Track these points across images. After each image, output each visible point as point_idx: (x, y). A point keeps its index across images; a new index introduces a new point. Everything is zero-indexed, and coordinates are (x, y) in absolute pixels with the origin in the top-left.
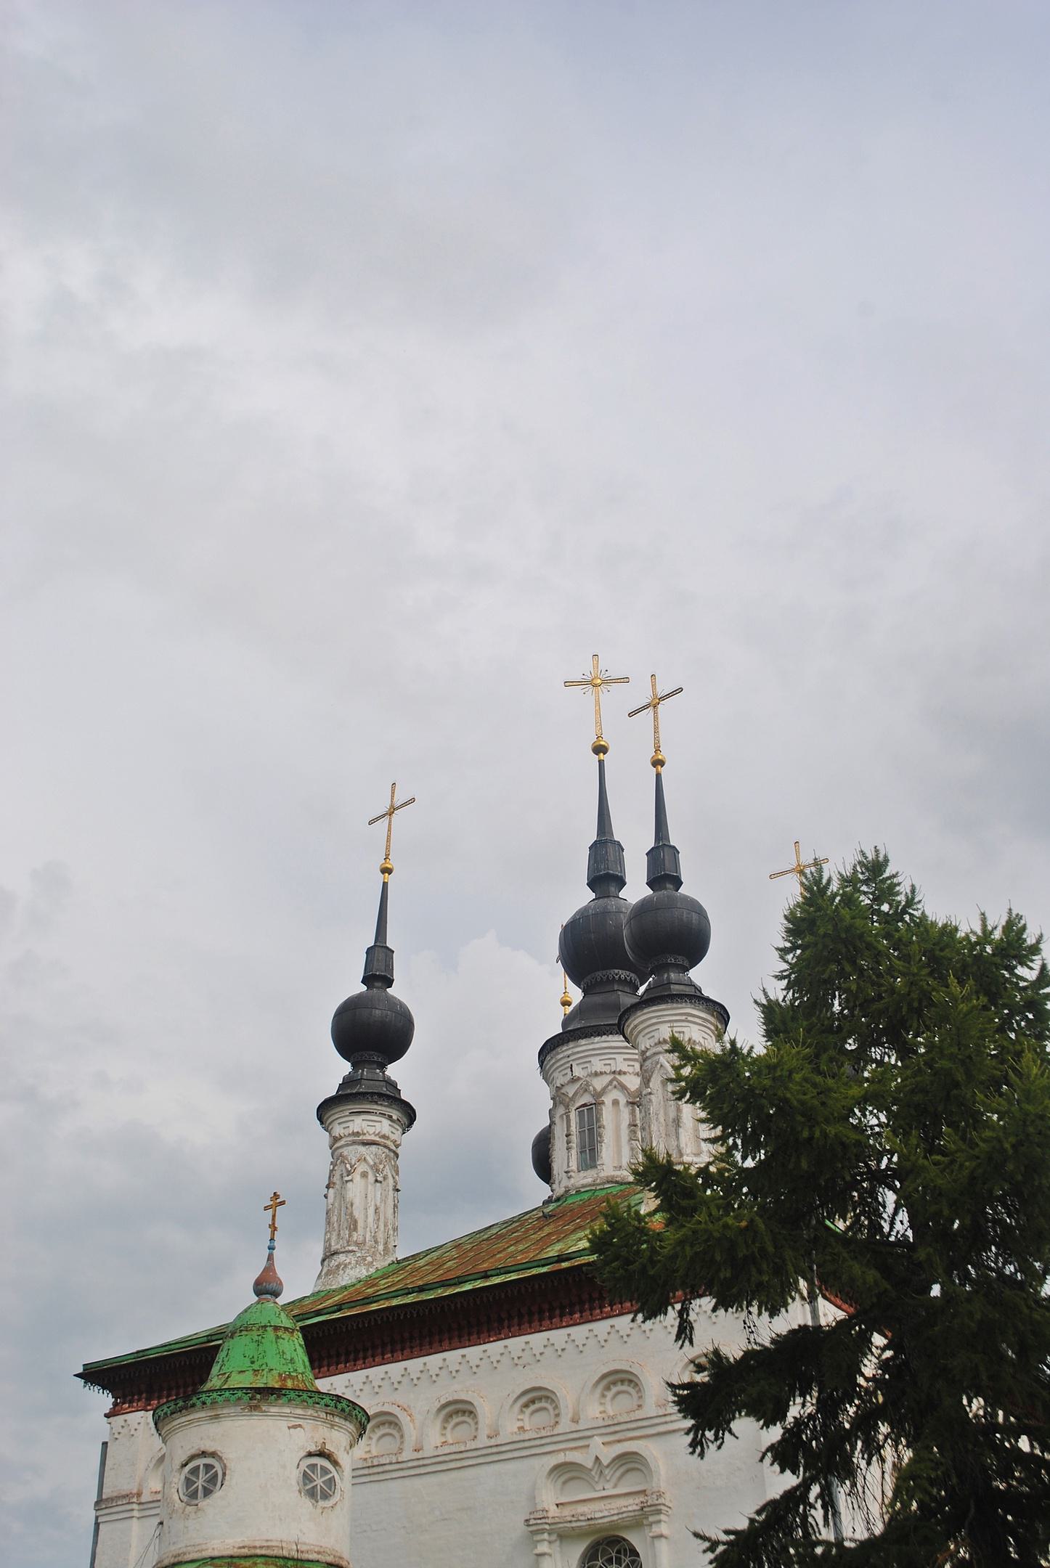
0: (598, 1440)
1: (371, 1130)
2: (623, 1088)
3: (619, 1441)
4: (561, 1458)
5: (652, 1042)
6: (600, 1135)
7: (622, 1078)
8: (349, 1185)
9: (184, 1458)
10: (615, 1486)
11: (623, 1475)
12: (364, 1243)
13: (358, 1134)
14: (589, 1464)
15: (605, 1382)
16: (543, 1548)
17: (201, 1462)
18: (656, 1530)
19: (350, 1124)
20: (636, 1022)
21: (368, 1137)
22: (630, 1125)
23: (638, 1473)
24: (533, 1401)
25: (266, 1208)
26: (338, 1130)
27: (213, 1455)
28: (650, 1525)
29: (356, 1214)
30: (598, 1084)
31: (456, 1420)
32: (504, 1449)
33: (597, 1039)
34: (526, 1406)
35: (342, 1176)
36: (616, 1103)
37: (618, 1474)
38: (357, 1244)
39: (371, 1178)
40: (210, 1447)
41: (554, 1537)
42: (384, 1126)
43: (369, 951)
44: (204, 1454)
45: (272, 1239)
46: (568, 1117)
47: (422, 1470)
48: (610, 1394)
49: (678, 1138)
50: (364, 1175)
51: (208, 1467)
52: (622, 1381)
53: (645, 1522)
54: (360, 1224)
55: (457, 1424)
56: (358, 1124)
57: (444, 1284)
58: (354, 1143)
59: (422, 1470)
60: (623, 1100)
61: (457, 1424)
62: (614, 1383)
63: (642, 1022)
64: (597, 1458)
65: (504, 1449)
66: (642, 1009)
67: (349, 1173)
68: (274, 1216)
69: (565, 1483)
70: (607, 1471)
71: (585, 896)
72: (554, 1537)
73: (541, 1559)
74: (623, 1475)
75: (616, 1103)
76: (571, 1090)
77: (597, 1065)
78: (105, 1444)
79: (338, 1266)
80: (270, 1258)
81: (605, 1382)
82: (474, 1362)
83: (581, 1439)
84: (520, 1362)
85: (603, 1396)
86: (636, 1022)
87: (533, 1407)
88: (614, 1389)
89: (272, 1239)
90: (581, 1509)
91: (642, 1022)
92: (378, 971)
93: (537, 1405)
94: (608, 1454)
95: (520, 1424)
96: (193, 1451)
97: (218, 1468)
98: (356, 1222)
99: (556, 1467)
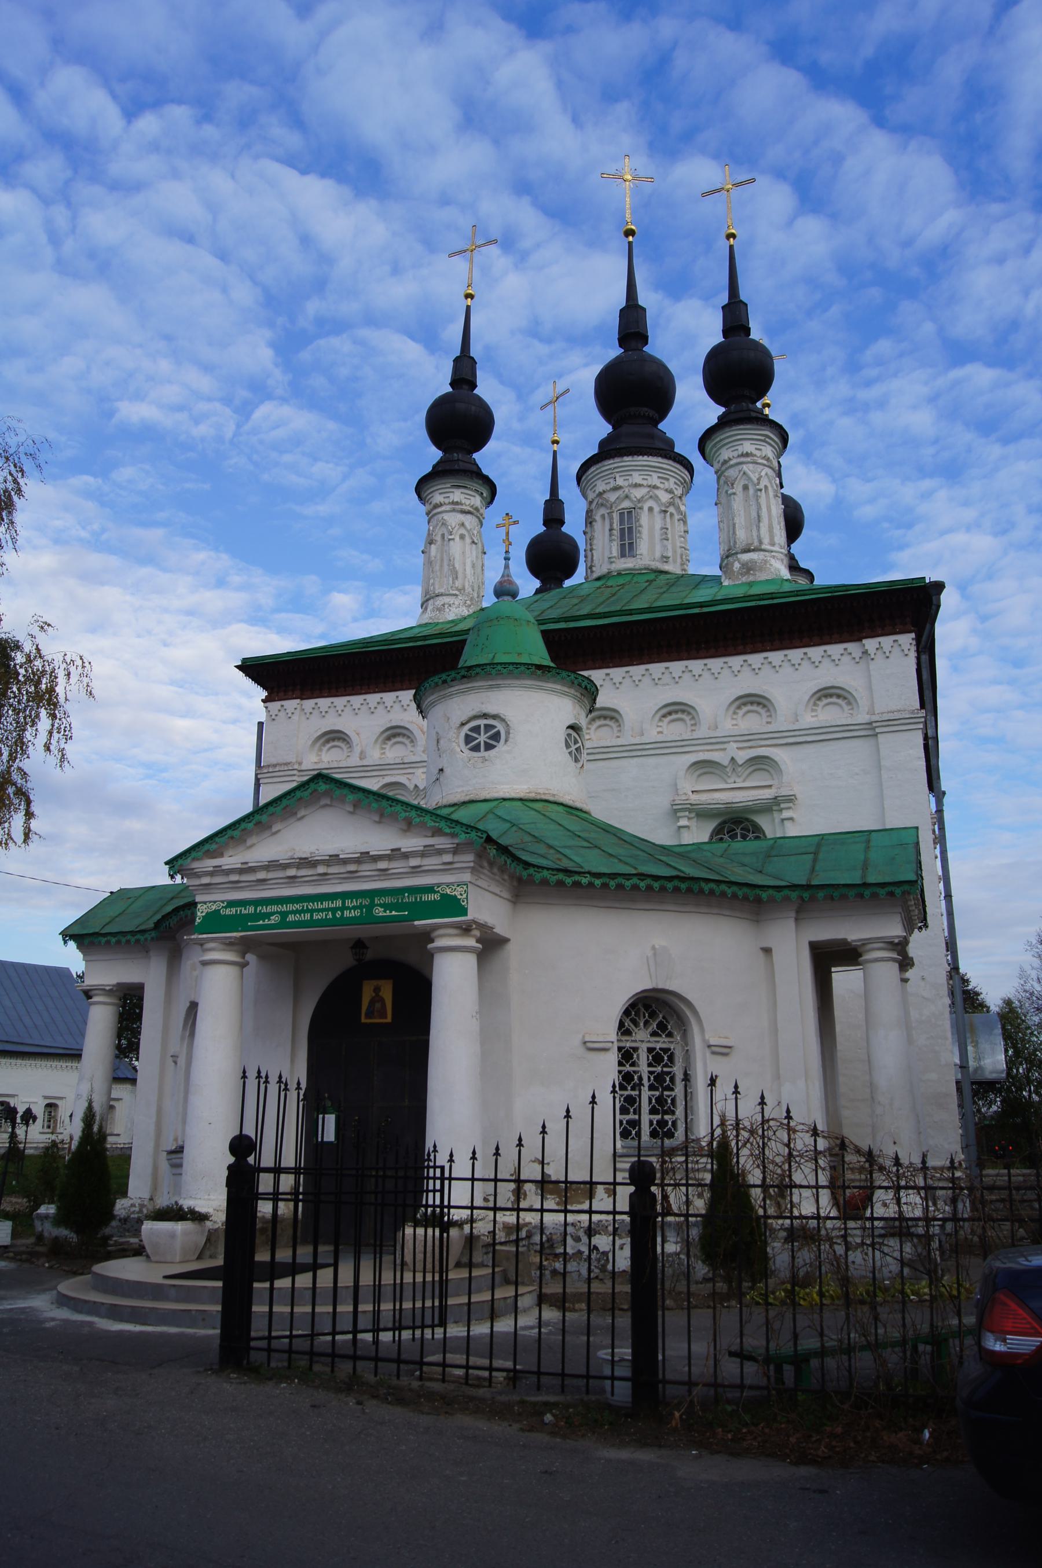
0: (735, 745)
1: (468, 502)
2: (656, 498)
3: (750, 747)
4: (702, 756)
5: (735, 454)
6: (640, 532)
7: (657, 492)
8: (451, 542)
9: (464, 718)
10: (744, 781)
11: (750, 773)
12: (464, 588)
13: (457, 503)
14: (725, 762)
15: (737, 703)
16: (683, 822)
17: (482, 722)
18: (786, 814)
19: (451, 495)
20: (722, 437)
21: (464, 507)
22: (662, 528)
23: (766, 773)
24: (670, 713)
25: (498, 526)
26: (438, 498)
27: (495, 717)
28: (781, 810)
29: (457, 566)
30: (638, 493)
31: (598, 723)
32: (648, 747)
33: (640, 458)
34: (664, 716)
35: (443, 536)
36: (651, 509)
37: (748, 772)
38: (459, 590)
39: (468, 540)
40: (491, 710)
41: (693, 815)
42: (477, 501)
43: (457, 361)
44: (485, 716)
45: (507, 552)
46: (611, 519)
47: (644, 753)
48: (741, 712)
49: (759, 531)
50: (462, 537)
51: (488, 727)
52: (752, 703)
53: (775, 808)
54: (460, 575)
55: (600, 726)
56: (457, 495)
57: (567, 619)
58: (454, 510)
59: (644, 753)
60: (656, 509)
61: (600, 726)
62: (745, 704)
63: (721, 440)
64: (733, 759)
65: (648, 747)
66: (731, 426)
67: (451, 534)
68: (507, 534)
69: (699, 776)
70: (740, 769)
71: (615, 352)
72: (693, 815)
73: (682, 830)
74: (750, 773)
75: (651, 509)
76: (612, 497)
77: (637, 478)
78: (261, 725)
79: (443, 605)
80: (507, 567)
81: (737, 703)
82: (656, 676)
83: (720, 743)
84: (660, 682)
85: (735, 713)
86: (722, 437)
87: (670, 718)
88: (745, 709)
89: (507, 552)
90: (717, 796)
91: (721, 440)
92: (464, 373)
93: (674, 716)
94: (742, 756)
95: (659, 729)
96: (474, 713)
97: (500, 727)
98: (457, 572)
99: (697, 764)
